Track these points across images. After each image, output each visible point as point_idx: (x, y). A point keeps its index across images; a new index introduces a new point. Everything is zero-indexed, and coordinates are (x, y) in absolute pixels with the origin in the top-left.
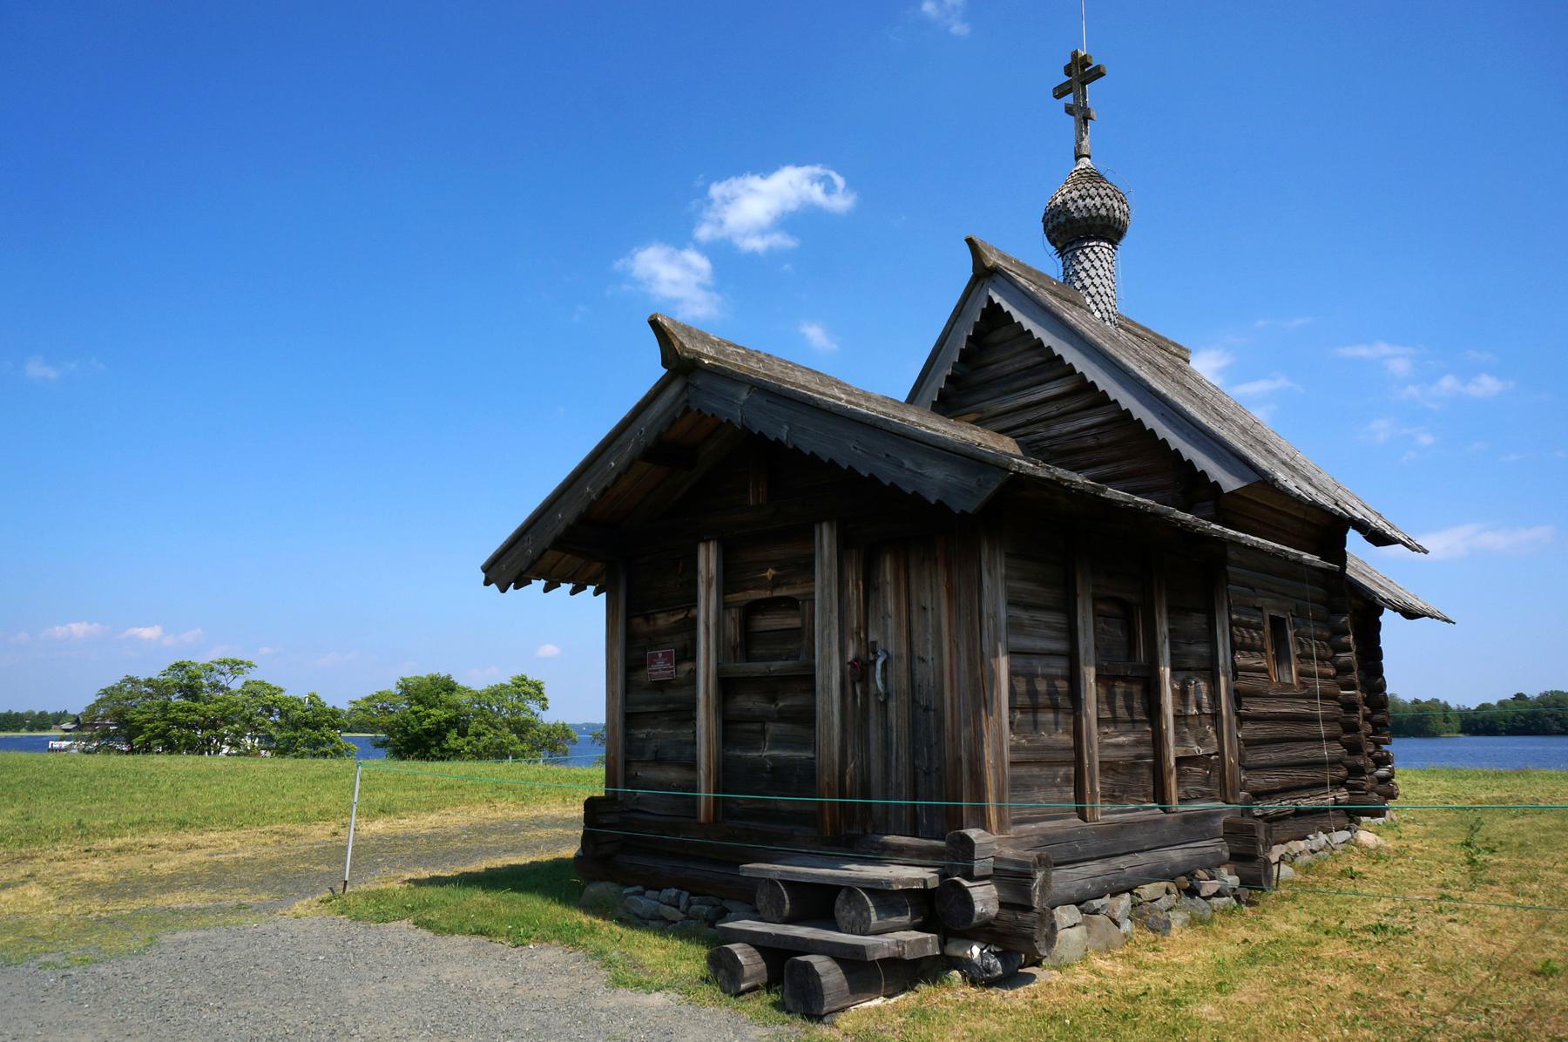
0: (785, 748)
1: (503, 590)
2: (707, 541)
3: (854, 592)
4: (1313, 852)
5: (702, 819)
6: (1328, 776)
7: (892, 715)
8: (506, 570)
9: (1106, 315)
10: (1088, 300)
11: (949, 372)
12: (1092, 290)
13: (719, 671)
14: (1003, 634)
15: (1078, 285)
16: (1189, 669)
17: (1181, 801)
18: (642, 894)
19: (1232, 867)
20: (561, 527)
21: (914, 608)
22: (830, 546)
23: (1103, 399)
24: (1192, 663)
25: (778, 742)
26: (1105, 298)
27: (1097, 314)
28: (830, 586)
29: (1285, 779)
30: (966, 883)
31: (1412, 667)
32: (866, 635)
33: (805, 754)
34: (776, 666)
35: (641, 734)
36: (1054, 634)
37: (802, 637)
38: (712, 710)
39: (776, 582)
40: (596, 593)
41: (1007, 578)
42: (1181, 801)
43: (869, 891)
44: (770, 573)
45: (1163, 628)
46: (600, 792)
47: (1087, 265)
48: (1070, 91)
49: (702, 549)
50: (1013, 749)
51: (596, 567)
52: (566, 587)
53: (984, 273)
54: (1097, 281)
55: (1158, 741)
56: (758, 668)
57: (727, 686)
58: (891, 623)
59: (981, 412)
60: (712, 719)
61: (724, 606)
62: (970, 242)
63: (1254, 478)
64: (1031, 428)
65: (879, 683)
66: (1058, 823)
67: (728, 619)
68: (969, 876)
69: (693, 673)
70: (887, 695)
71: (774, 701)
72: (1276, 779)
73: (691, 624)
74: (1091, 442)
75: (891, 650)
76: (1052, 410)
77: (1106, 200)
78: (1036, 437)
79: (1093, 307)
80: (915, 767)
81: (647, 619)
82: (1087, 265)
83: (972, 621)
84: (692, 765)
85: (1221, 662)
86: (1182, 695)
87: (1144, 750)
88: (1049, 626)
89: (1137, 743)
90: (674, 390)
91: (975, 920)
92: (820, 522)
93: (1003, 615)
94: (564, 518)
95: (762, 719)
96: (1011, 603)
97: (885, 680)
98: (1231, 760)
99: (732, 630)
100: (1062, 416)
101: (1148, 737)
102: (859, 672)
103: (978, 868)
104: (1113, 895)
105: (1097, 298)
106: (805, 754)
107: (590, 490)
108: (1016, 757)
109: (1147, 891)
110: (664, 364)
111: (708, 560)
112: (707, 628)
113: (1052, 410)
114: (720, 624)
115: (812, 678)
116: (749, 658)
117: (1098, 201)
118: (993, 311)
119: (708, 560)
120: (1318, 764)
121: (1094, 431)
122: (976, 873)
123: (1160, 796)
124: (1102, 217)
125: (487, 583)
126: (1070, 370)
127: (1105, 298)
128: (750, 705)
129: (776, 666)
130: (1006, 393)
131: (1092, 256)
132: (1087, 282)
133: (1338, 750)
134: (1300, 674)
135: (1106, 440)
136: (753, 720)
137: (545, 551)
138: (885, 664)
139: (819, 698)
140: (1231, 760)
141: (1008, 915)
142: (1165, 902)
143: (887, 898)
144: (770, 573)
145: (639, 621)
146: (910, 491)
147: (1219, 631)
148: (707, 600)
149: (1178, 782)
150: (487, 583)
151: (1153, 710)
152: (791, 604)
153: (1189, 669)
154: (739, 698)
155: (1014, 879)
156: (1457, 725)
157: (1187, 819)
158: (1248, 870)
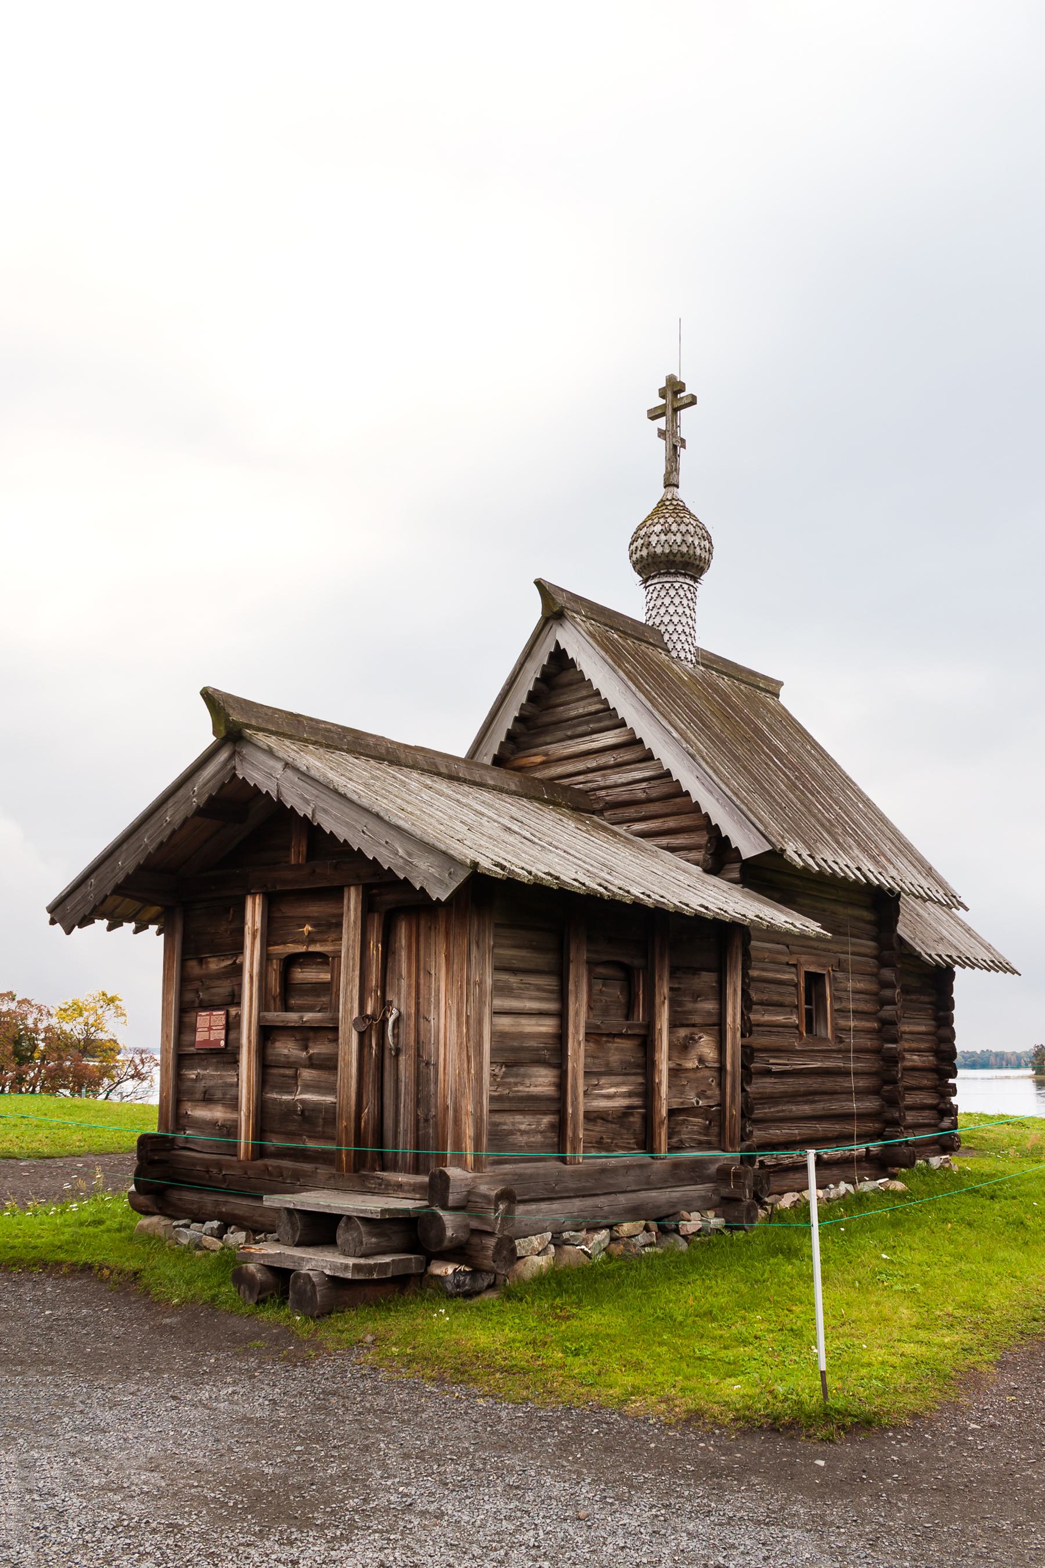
0: (313, 1093)
2: (254, 895)
3: (375, 950)
5: (242, 1156)
6: (855, 1128)
7: (402, 1067)
8: (71, 910)
14: (488, 998)
16: (694, 1025)
18: (187, 1226)
20: (120, 878)
22: (356, 910)
24: (697, 1019)
25: (308, 1088)
27: (674, 654)
28: (354, 948)
30: (441, 1213)
33: (330, 1099)
35: (192, 1074)
36: (544, 995)
37: (328, 989)
38: (253, 1053)
39: (311, 940)
40: (159, 933)
42: (671, 1149)
44: (308, 928)
45: (663, 989)
46: (153, 1129)
48: (663, 414)
50: (492, 1099)
51: (155, 910)
53: (556, 608)
55: (648, 1093)
57: (267, 1033)
58: (404, 983)
59: (546, 755)
61: (266, 958)
64: (590, 776)
65: (390, 1038)
68: (445, 1207)
73: (237, 970)
76: (609, 759)
79: (670, 646)
81: (201, 961)
83: (461, 986)
85: (729, 1020)
86: (681, 1048)
88: (539, 988)
89: (630, 1095)
90: (223, 756)
91: (446, 1243)
92: (349, 886)
93: (489, 982)
94: (126, 864)
96: (497, 969)
97: (396, 1036)
103: (452, 1199)
104: (589, 1230)
106: (330, 1099)
107: (148, 841)
108: (496, 1107)
109: (626, 1228)
111: (254, 913)
112: (251, 977)
113: (609, 759)
115: (336, 1029)
116: (287, 1008)
118: (560, 658)
119: (254, 913)
120: (846, 1117)
121: (644, 785)
122: (450, 1203)
123: (647, 1143)
124: (683, 555)
125: (53, 922)
128: (286, 1052)
129: (308, 1016)
130: (571, 738)
135: (654, 793)
136: (289, 1065)
137: (106, 897)
142: (641, 1239)
144: (308, 928)
145: (193, 963)
146: (402, 876)
147: (729, 991)
148: (252, 952)
149: (670, 1136)
150: (53, 922)
151: (647, 1066)
152: (322, 960)
153: (694, 1025)
157: (676, 1165)
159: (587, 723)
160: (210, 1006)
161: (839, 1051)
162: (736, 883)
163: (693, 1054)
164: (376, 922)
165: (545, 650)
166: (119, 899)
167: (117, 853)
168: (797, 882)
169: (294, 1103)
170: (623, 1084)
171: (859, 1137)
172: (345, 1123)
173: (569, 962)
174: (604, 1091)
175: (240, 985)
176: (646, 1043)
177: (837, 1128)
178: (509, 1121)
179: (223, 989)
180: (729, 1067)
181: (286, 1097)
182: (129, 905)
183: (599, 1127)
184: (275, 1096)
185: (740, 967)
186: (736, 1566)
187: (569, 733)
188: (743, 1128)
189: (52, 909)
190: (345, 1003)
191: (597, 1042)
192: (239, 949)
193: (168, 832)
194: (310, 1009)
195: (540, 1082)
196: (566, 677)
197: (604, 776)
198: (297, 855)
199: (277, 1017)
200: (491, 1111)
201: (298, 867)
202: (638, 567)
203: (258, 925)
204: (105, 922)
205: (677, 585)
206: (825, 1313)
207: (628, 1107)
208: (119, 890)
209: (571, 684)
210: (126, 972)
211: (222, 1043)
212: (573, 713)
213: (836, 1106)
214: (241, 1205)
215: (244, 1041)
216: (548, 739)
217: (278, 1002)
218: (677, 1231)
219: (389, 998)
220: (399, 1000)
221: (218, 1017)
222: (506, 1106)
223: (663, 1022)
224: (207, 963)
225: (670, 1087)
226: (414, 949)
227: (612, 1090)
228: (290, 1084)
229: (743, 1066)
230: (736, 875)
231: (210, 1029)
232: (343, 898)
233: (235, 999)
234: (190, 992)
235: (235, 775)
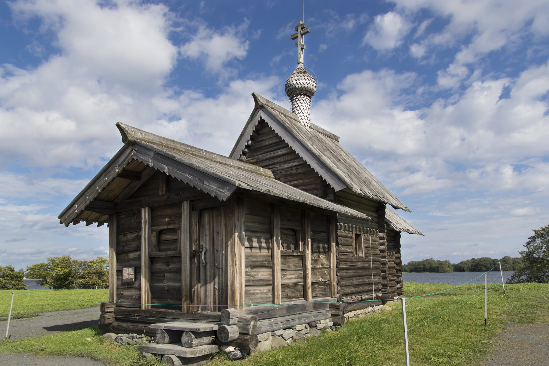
1: (67, 225)
3: (195, 227)
4: (366, 313)
8: (70, 217)
9: (306, 124)
10: (300, 118)
12: (301, 114)
15: (297, 112)
17: (313, 297)
19: (331, 319)
20: (88, 202)
21: (215, 233)
23: (297, 157)
25: (170, 280)
26: (306, 118)
27: (303, 124)
29: (356, 289)
31: (410, 251)
32: (199, 242)
33: (177, 284)
34: (169, 253)
38: (147, 268)
39: (169, 223)
41: (245, 222)
43: (191, 332)
44: (167, 219)
47: (300, 105)
50: (246, 281)
51: (106, 217)
53: (259, 107)
54: (303, 111)
55: (305, 277)
56: (163, 254)
57: (152, 260)
60: (147, 273)
61: (151, 231)
63: (345, 187)
65: (203, 259)
66: (263, 305)
67: (153, 236)
68: (229, 325)
69: (140, 256)
70: (206, 263)
72: (353, 289)
73: (139, 238)
75: (208, 247)
77: (307, 81)
78: (276, 169)
79: (301, 121)
81: (124, 235)
82: (300, 105)
86: (315, 261)
87: (299, 280)
89: (298, 278)
94: (89, 198)
95: (164, 272)
97: (205, 258)
98: (334, 283)
99: (154, 239)
100: (285, 162)
101: (302, 275)
102: (194, 255)
103: (231, 322)
105: (303, 118)
108: (248, 284)
110: (123, 142)
111: (145, 214)
112: (145, 239)
114: (149, 238)
115: (180, 257)
117: (304, 81)
118: (262, 122)
119: (145, 214)
121: (295, 168)
123: (305, 296)
126: (287, 145)
127: (306, 118)
128: (160, 267)
129: (169, 253)
131: (302, 101)
132: (300, 111)
133: (379, 279)
134: (366, 253)
138: (205, 253)
139: (183, 265)
140: (334, 283)
141: (242, 336)
143: (198, 334)
144: (167, 219)
145: (122, 236)
149: (313, 292)
152: (174, 231)
154: (157, 265)
155: (243, 324)
156: (452, 269)
158: (337, 319)
159: (273, 146)
161: (367, 261)
163: (319, 262)
165: (257, 119)
166: (90, 212)
167: (86, 193)
168: (351, 202)
169: (164, 287)
170: (294, 274)
171: (375, 290)
173: (274, 228)
175: (140, 243)
176: (303, 258)
177: (367, 288)
178: (252, 289)
179: (134, 245)
180: (332, 267)
181: (161, 284)
182: (95, 215)
183: (287, 290)
184: (156, 284)
187: (266, 151)
188: (337, 289)
189: (60, 217)
190: (184, 247)
191: (285, 258)
192: (140, 229)
194: (169, 250)
195: (263, 274)
196: (265, 130)
198: (161, 191)
199: (156, 254)
200: (246, 286)
201: (163, 195)
202: (289, 93)
204: (85, 222)
205: (304, 99)
206: (410, 361)
207: (297, 283)
208: (88, 208)
209: (266, 133)
210: (94, 242)
213: (366, 280)
214: (143, 326)
215: (143, 264)
216: (258, 153)
217: (156, 248)
218: (316, 327)
219: (201, 243)
220: (206, 243)
222: (251, 283)
223: (309, 252)
225: (312, 274)
226: (211, 226)
227: (291, 276)
229: (337, 267)
230: (332, 198)
232: (181, 206)
234: (123, 248)
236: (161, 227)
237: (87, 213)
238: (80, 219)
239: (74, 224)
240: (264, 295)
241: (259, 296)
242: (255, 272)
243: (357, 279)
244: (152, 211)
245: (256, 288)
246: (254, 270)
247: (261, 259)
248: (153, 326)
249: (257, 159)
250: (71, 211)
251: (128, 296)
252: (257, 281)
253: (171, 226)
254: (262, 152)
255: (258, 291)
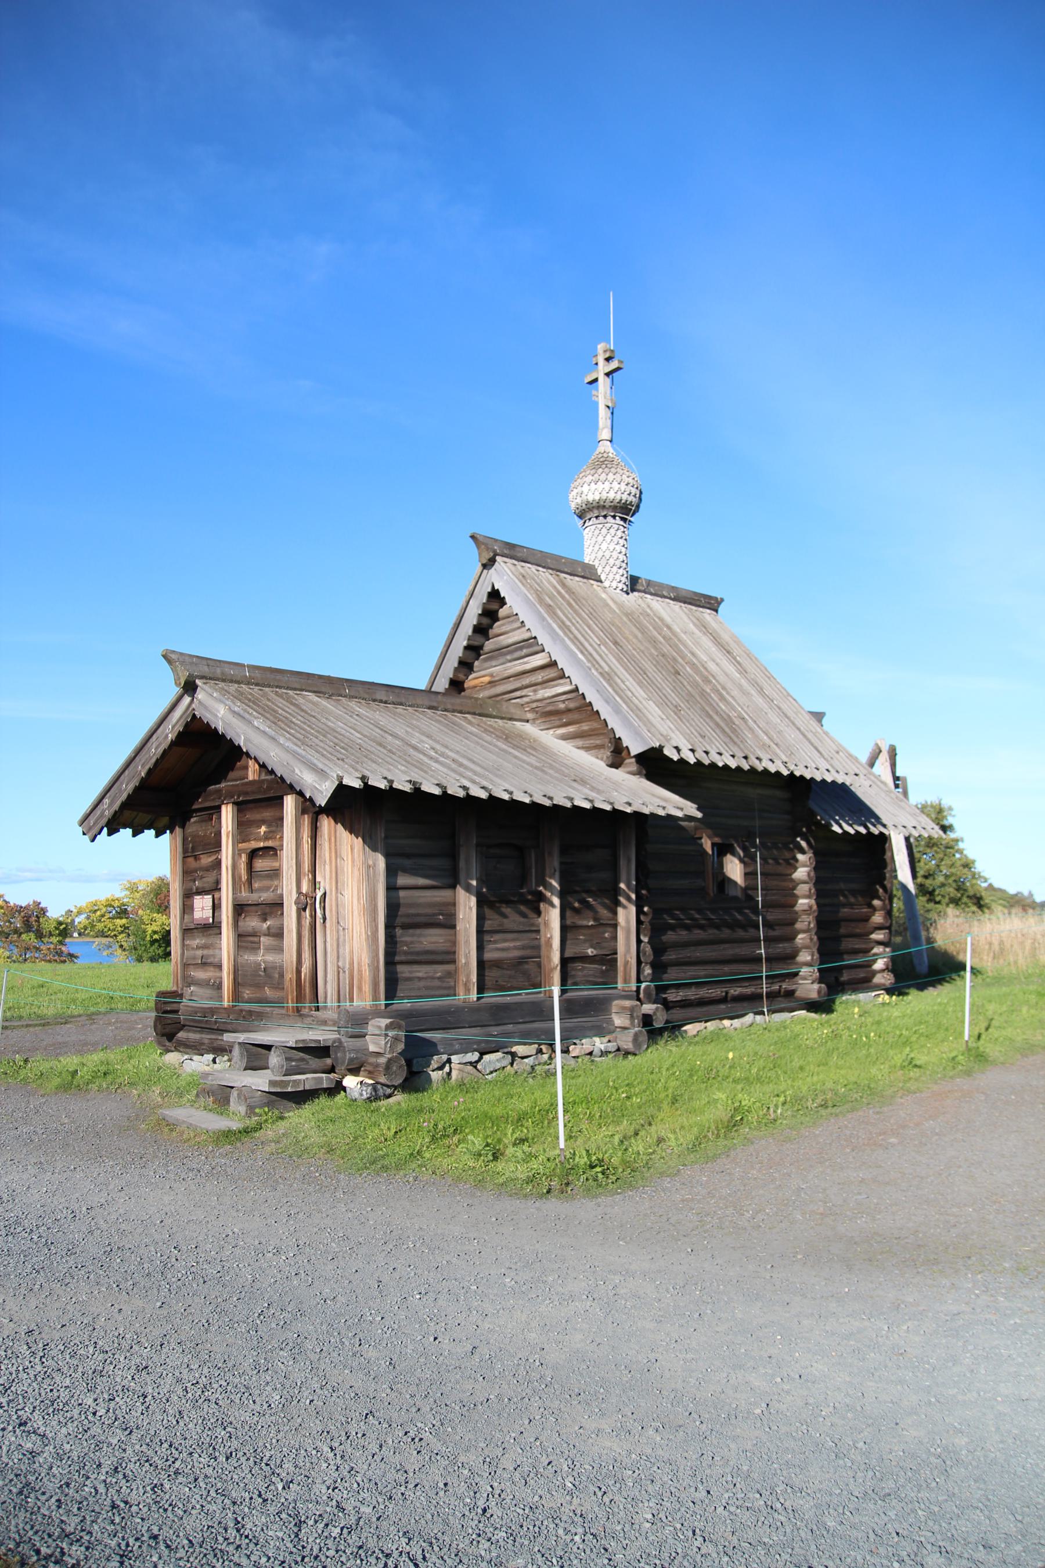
11: (465, 643)
13: (234, 899)
20: (124, 796)
37: (276, 874)
44: (263, 829)
49: (224, 808)
51: (165, 820)
52: (150, 833)
57: (240, 909)
58: (327, 867)
62: (472, 537)
71: (265, 920)
73: (218, 863)
74: (562, 706)
80: (338, 967)
81: (196, 858)
84: (220, 967)
90: (187, 699)
94: (127, 787)
111: (227, 814)
113: (539, 677)
119: (227, 814)
121: (564, 697)
145: (191, 860)
147: (623, 863)
160: (201, 892)
162: (634, 774)
164: (306, 820)
172: (290, 975)
174: (498, 946)
179: (210, 879)
182: (143, 817)
185: (633, 843)
186: (1042, 1460)
189: (82, 823)
193: (154, 760)
197: (535, 691)
199: (245, 895)
203: (230, 828)
204: (152, 832)
208: (124, 806)
211: (211, 920)
212: (511, 641)
216: (494, 663)
221: (208, 900)
224: (200, 859)
227: (506, 945)
228: (255, 948)
231: (203, 909)
233: (216, 888)
235: (194, 715)
236: (254, 845)
237: (127, 814)
238: (119, 824)
239: (110, 834)
240: (437, 983)
241: (422, 984)
242: (413, 935)
243: (344, 946)
244: (241, 807)
245: (415, 968)
246: (411, 931)
247: (429, 911)
248: (227, 1037)
249: (491, 675)
250: (98, 812)
251: (203, 980)
252: (418, 953)
253: (269, 844)
254: (502, 660)
255: (420, 975)
